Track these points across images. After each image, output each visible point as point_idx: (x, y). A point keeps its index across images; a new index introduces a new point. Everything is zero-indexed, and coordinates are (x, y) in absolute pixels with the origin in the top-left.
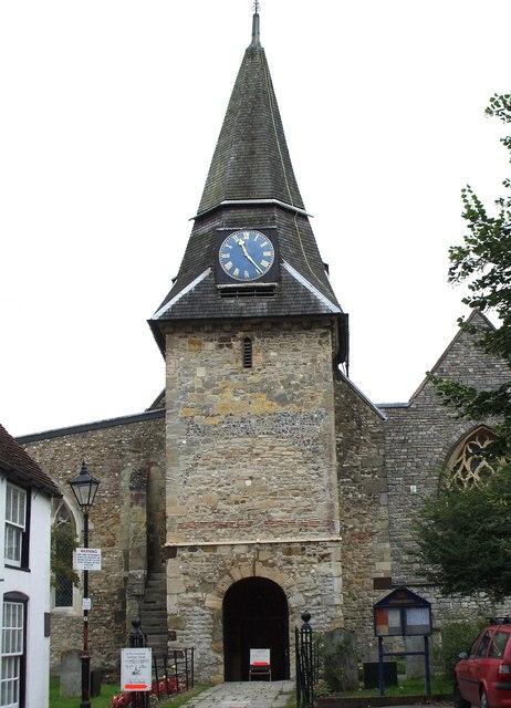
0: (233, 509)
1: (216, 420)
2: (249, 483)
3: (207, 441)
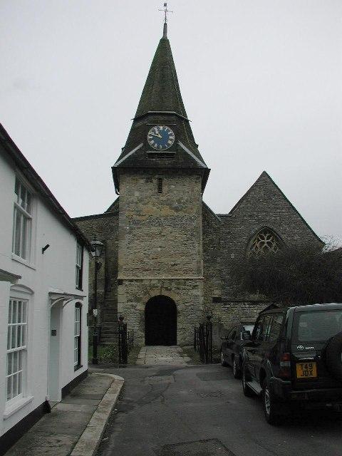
0: (151, 262)
1: (144, 218)
2: (159, 249)
3: (140, 228)
